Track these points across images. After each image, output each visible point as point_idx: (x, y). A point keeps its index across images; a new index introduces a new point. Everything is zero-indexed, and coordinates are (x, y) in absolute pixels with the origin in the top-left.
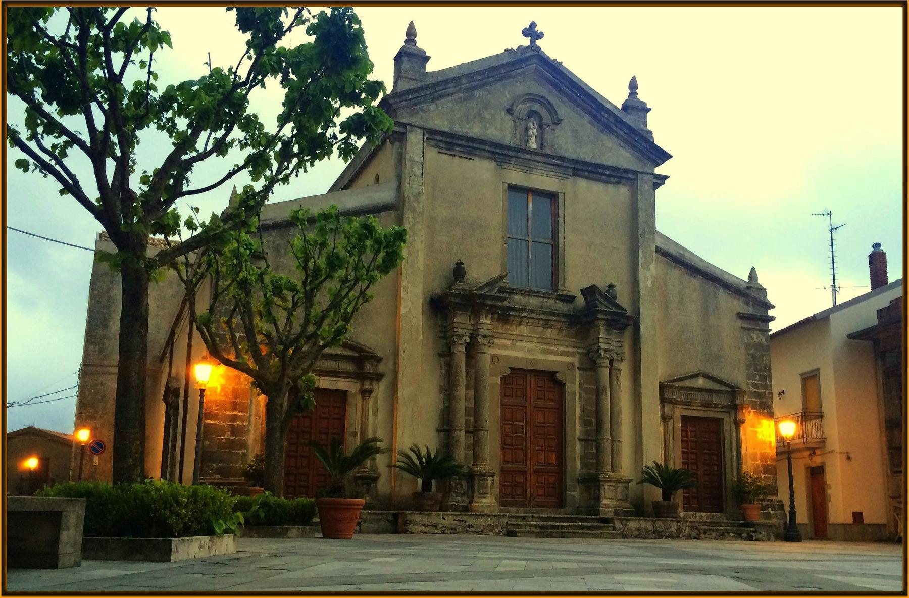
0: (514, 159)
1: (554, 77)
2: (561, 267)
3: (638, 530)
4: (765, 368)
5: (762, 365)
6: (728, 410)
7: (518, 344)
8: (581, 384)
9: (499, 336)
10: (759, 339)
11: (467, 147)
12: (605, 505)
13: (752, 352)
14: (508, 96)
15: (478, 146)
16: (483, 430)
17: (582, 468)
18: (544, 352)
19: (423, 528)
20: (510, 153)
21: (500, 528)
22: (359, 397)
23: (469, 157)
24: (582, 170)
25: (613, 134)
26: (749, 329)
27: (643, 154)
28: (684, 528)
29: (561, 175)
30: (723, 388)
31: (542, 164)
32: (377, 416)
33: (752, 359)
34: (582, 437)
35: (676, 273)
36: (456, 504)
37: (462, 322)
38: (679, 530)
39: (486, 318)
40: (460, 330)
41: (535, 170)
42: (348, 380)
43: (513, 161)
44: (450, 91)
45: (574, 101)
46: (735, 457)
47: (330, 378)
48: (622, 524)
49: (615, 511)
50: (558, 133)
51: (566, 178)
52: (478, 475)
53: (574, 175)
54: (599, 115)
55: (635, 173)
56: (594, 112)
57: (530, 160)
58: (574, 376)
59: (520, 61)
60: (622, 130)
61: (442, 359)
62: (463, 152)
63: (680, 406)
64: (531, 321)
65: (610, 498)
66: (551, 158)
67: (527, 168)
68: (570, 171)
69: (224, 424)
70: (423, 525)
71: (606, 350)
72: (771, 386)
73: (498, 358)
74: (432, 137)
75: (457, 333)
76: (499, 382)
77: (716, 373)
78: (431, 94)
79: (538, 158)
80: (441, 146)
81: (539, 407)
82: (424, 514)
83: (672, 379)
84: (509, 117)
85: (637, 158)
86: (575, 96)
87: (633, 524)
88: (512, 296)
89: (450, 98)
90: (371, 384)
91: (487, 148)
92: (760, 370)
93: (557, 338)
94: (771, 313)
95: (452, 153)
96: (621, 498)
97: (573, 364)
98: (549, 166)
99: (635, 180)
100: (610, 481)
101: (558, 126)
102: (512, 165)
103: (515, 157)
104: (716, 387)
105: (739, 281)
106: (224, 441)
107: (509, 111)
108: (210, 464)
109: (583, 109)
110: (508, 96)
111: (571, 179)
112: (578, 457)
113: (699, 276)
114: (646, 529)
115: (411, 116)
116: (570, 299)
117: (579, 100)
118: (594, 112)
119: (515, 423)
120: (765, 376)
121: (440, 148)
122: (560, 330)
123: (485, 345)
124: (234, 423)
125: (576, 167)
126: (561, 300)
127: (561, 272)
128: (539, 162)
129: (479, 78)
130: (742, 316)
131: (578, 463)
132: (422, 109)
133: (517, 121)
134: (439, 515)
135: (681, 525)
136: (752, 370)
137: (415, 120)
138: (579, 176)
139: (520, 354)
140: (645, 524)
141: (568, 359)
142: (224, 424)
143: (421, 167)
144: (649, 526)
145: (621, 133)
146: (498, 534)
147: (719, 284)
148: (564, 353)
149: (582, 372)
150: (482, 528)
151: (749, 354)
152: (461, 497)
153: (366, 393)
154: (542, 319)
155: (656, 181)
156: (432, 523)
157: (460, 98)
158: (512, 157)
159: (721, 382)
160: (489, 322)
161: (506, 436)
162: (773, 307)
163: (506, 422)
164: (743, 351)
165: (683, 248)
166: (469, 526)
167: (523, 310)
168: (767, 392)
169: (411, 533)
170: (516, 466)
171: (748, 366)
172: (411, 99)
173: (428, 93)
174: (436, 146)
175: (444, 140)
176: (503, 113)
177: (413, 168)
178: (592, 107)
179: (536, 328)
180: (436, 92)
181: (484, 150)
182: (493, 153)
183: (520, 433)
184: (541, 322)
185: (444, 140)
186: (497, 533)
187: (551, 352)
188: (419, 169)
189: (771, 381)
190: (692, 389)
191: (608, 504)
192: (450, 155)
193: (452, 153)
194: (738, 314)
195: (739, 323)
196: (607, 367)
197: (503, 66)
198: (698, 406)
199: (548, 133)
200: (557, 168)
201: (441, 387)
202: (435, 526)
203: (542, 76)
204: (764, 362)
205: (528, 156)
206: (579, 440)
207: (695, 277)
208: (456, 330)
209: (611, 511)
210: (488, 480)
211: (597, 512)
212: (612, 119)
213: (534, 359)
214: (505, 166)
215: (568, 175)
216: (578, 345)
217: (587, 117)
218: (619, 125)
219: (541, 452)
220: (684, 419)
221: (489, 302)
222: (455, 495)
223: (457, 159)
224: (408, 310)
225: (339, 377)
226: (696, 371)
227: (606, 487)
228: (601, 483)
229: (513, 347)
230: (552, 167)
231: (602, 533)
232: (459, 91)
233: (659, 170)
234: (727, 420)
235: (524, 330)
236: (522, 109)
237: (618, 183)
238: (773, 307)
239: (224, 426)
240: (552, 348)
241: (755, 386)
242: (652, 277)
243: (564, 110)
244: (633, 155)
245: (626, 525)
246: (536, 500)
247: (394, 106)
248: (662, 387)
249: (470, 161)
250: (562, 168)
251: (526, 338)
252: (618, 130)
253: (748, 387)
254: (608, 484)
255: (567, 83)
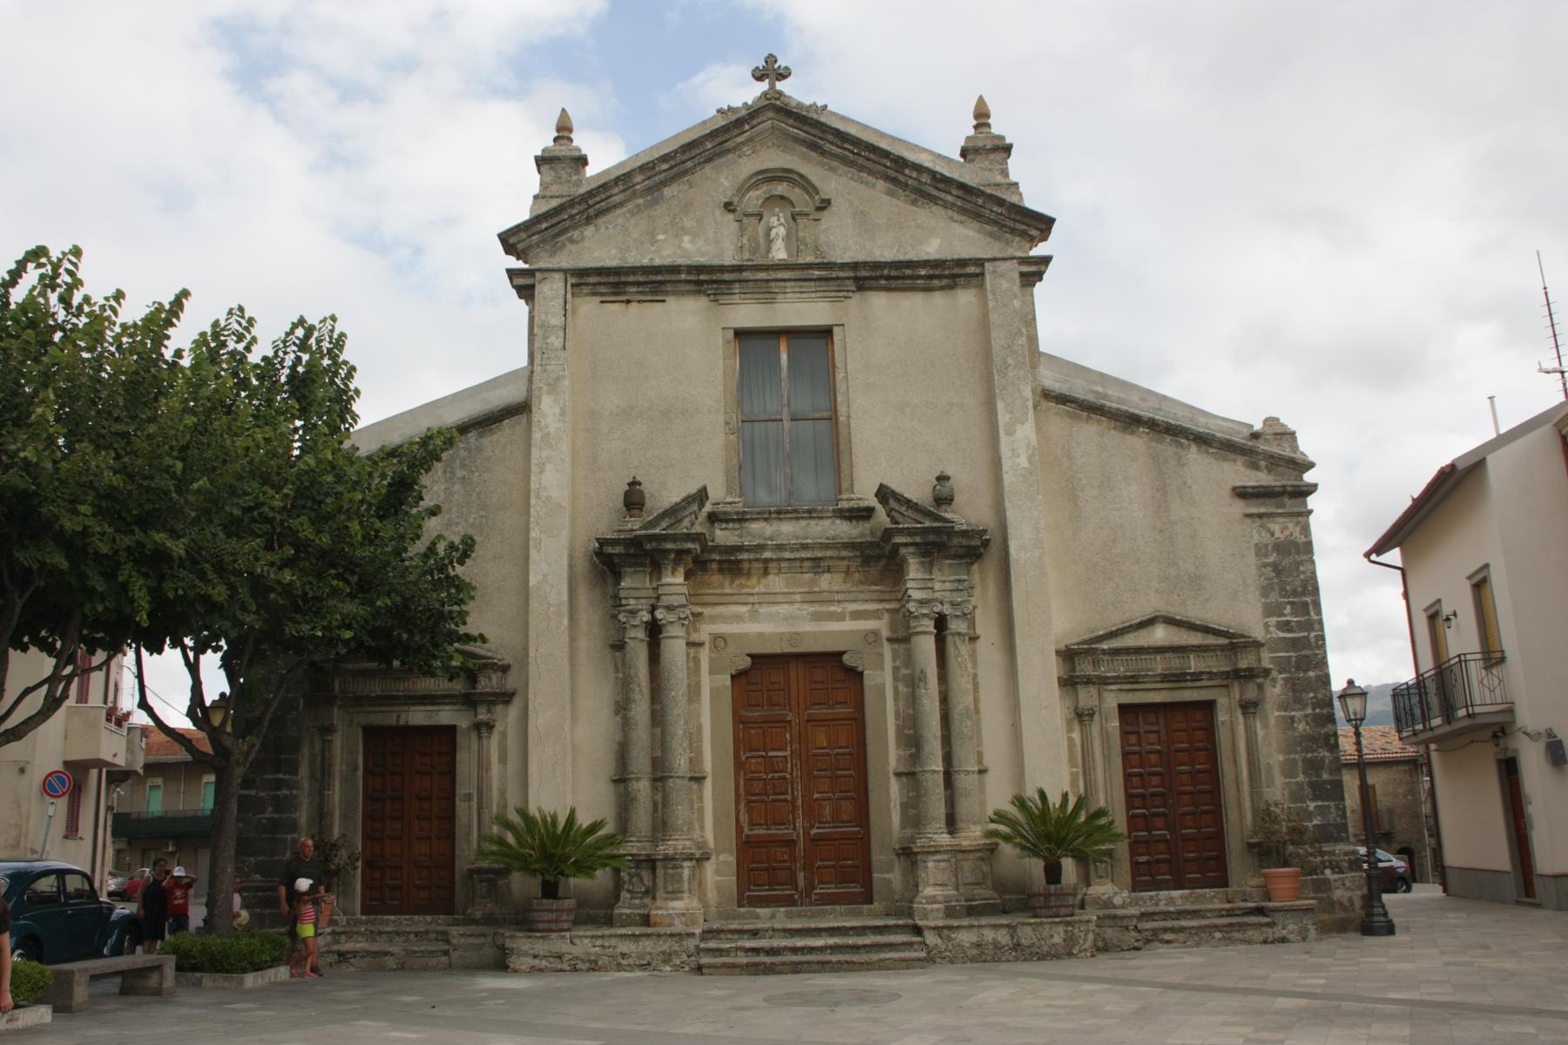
0: (737, 285)
1: (805, 132)
2: (844, 457)
3: (978, 945)
4: (1305, 587)
5: (1298, 583)
6: (1225, 682)
7: (764, 610)
8: (896, 670)
9: (726, 599)
10: (1287, 533)
11: (646, 283)
12: (926, 898)
13: (1271, 559)
14: (726, 183)
15: (668, 277)
16: (672, 777)
17: (903, 827)
18: (817, 617)
19: (536, 962)
20: (727, 277)
21: (684, 957)
22: (474, 735)
23: (656, 298)
24: (871, 278)
25: (936, 204)
26: (1260, 516)
27: (1002, 226)
28: (1082, 935)
29: (833, 294)
30: (1211, 640)
31: (792, 284)
32: (506, 764)
33: (1273, 574)
34: (902, 769)
35: (1090, 433)
36: (628, 911)
37: (634, 583)
38: (1070, 940)
39: (673, 574)
40: (632, 602)
41: (782, 296)
42: (455, 708)
43: (737, 288)
44: (616, 199)
45: (852, 164)
46: (1245, 774)
47: (423, 708)
48: (941, 938)
49: (946, 908)
50: (824, 224)
51: (846, 297)
52: (661, 860)
53: (860, 289)
54: (901, 178)
55: (980, 262)
56: (892, 173)
57: (767, 281)
58: (881, 655)
59: (739, 123)
60: (950, 193)
61: (617, 654)
62: (642, 293)
63: (1114, 687)
64: (784, 565)
65: (940, 885)
66: (807, 269)
67: (766, 296)
68: (851, 286)
69: (263, 794)
70: (535, 957)
71: (922, 602)
72: (1320, 622)
73: (725, 640)
74: (582, 281)
75: (627, 607)
76: (728, 683)
77: (1195, 613)
78: (581, 212)
79: (780, 275)
80: (603, 291)
81: (816, 721)
82: (536, 937)
83: (1092, 635)
84: (731, 217)
85: (991, 235)
86: (850, 155)
87: (966, 938)
88: (747, 525)
89: (619, 211)
90: (489, 711)
91: (683, 276)
92: (1294, 593)
93: (844, 587)
94: (1309, 477)
95: (624, 298)
96: (971, 880)
97: (876, 633)
98: (806, 284)
99: (982, 274)
100: (938, 852)
101: (825, 212)
102: (737, 296)
103: (740, 281)
104: (1195, 639)
105: (1231, 425)
106: (264, 821)
107: (729, 207)
108: (245, 858)
109: (871, 172)
110: (726, 183)
111: (857, 296)
112: (895, 806)
113: (1141, 430)
114: (996, 944)
115: (553, 253)
116: (865, 514)
117: (861, 161)
118: (892, 173)
119: (771, 754)
120: (1306, 603)
121: (602, 294)
122: (847, 572)
123: (672, 622)
124: (279, 793)
125: (858, 274)
126: (841, 517)
127: (844, 466)
128: (785, 280)
129: (665, 166)
130: (1242, 493)
131: (896, 818)
132: (571, 241)
133: (745, 220)
134: (563, 937)
135: (1076, 931)
136: (1274, 597)
137: (558, 260)
138: (870, 289)
139: (767, 628)
140: (992, 932)
141: (871, 624)
142: (263, 794)
143: (562, 334)
144: (1003, 937)
145: (949, 198)
146: (677, 968)
147: (1188, 439)
148: (857, 615)
149: (896, 646)
150: (648, 958)
151: (1265, 565)
152: (641, 898)
153: (483, 728)
154: (808, 559)
155: (1025, 269)
156: (550, 952)
157: (638, 206)
158: (731, 282)
159: (1206, 630)
160: (680, 579)
161: (752, 779)
162: (1311, 465)
163: (754, 753)
164: (1251, 558)
165: (1103, 377)
166: (623, 955)
167: (762, 547)
168: (1313, 635)
169: (515, 971)
170: (774, 832)
171: (1265, 591)
172: (546, 229)
173: (575, 211)
174: (594, 294)
175: (604, 280)
176: (718, 213)
177: (548, 338)
178: (886, 166)
179: (799, 575)
180: (590, 207)
181: (679, 281)
182: (699, 283)
183: (781, 771)
184: (806, 564)
185: (604, 280)
186: (678, 966)
187: (831, 617)
188: (557, 337)
189: (1319, 612)
190: (1139, 650)
191: (934, 897)
192: (622, 302)
193: (624, 298)
194: (1234, 489)
195: (1240, 507)
196: (930, 633)
197: (713, 134)
198: (1156, 682)
199: (805, 227)
200: (823, 283)
201: (617, 702)
202: (560, 957)
203: (788, 136)
204: (1302, 577)
205: (762, 275)
206: (898, 775)
207: (1132, 433)
208: (624, 602)
209: (937, 910)
210: (682, 867)
211: (910, 913)
212: (925, 178)
213: (796, 633)
214: (724, 299)
215: (848, 291)
216: (887, 596)
217: (881, 184)
218: (942, 186)
219: (825, 803)
220: (1123, 708)
221: (670, 546)
222: (628, 896)
223: (634, 307)
224: (541, 578)
225: (439, 704)
226: (1147, 613)
227: (930, 864)
228: (919, 857)
229: (754, 616)
230: (813, 284)
231: (881, 960)
232: (634, 196)
233: (1040, 250)
234: (1222, 702)
235: (776, 582)
236: (754, 198)
237: (951, 287)
238: (1311, 465)
239: (263, 797)
240: (832, 609)
241: (1285, 626)
242: (1028, 448)
243: (833, 182)
244: (979, 231)
245: (950, 939)
246: (818, 891)
247: (519, 246)
248: (1068, 655)
249: (660, 304)
250: (832, 283)
251: (780, 598)
252: (943, 195)
253: (1268, 632)
254: (935, 858)
255: (830, 138)
